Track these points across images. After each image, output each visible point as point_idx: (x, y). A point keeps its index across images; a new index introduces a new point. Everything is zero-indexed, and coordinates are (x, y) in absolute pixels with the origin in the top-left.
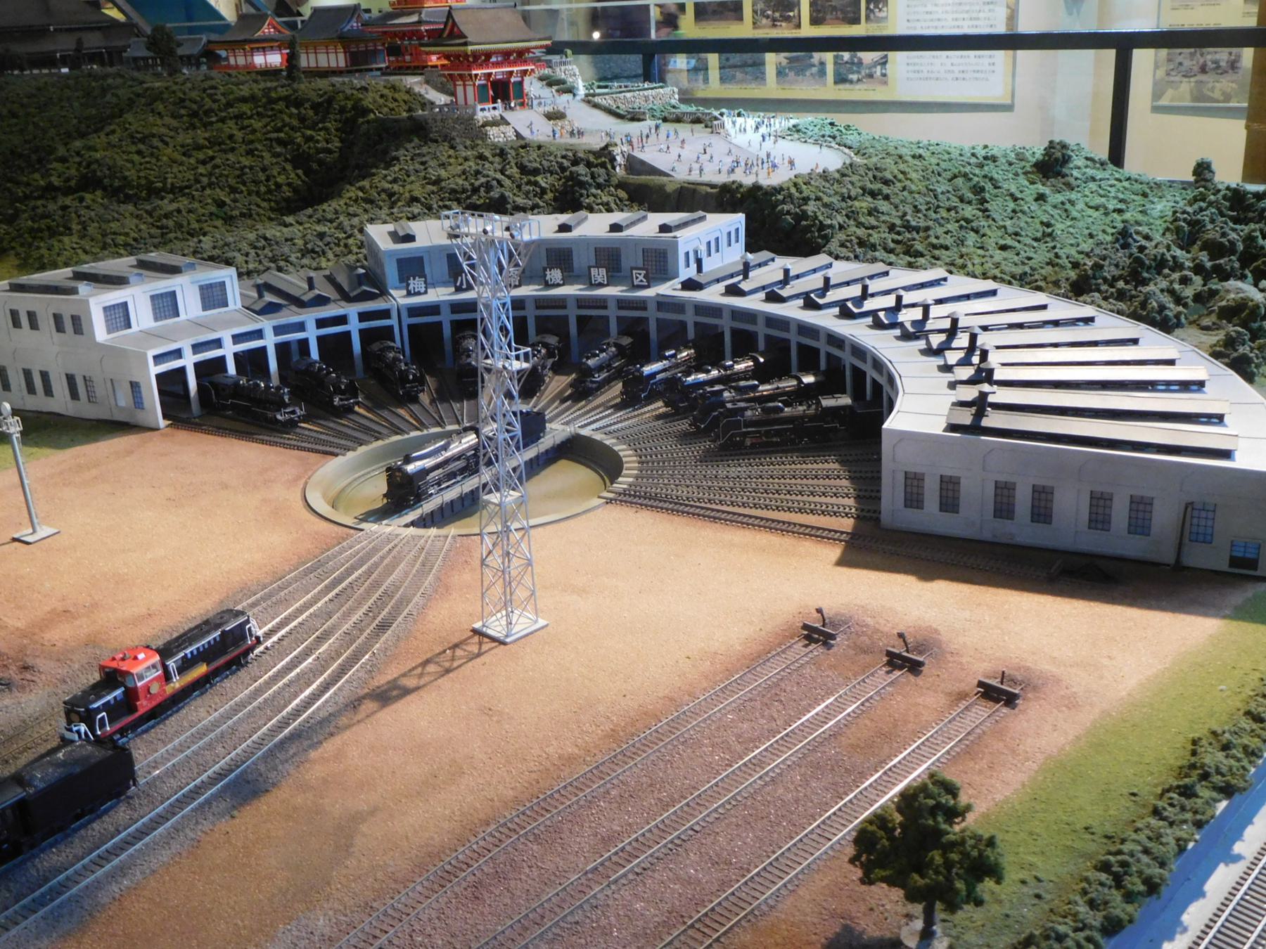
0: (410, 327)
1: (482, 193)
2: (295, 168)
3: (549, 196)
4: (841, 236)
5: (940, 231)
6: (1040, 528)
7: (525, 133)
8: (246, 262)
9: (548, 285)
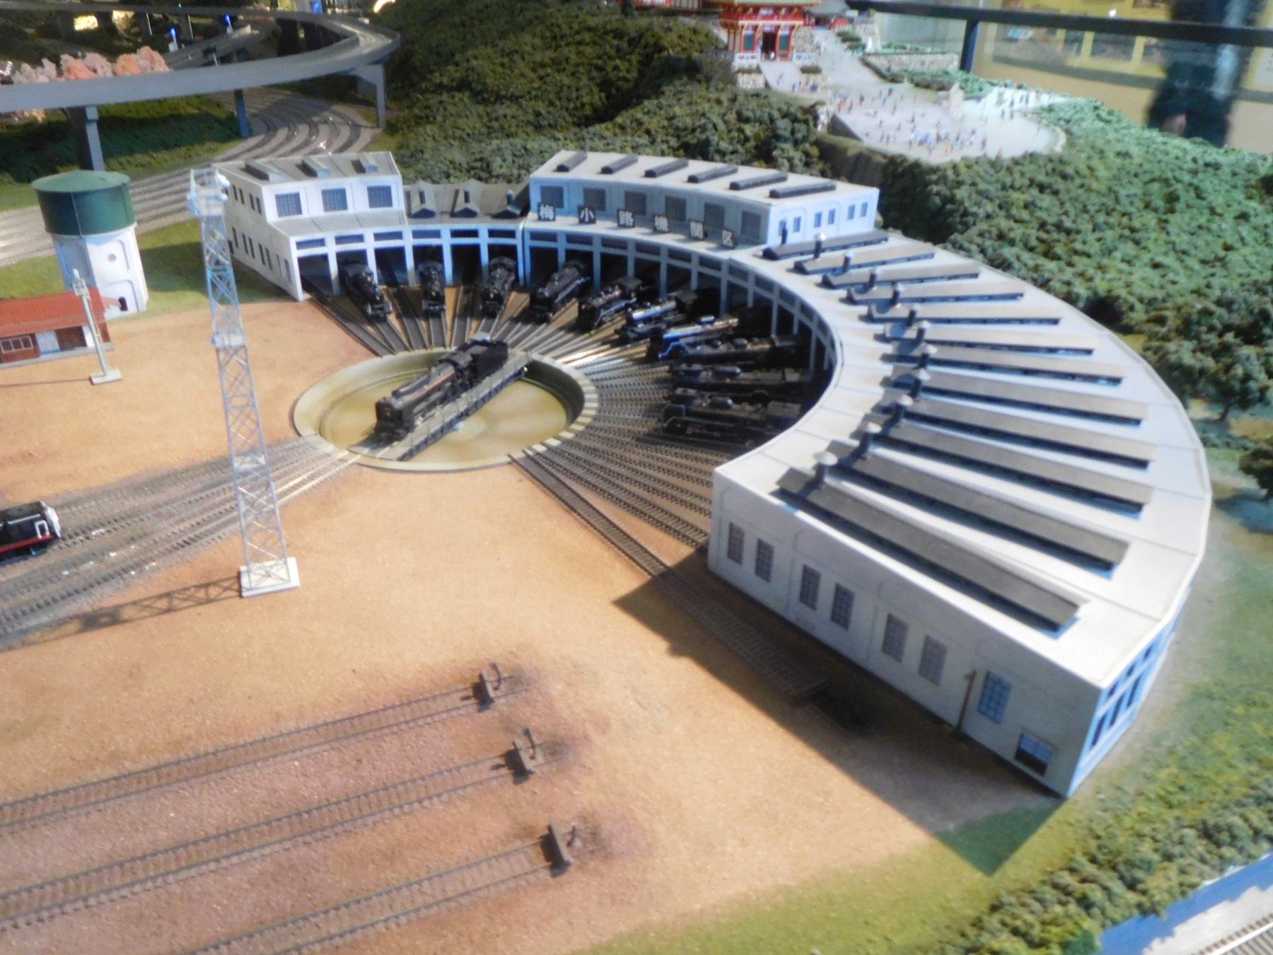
0: (533, 250)
1: (697, 133)
2: (601, 91)
3: (752, 143)
4: (983, 226)
5: (1092, 237)
6: (837, 628)
7: (772, 83)
9: (656, 231)
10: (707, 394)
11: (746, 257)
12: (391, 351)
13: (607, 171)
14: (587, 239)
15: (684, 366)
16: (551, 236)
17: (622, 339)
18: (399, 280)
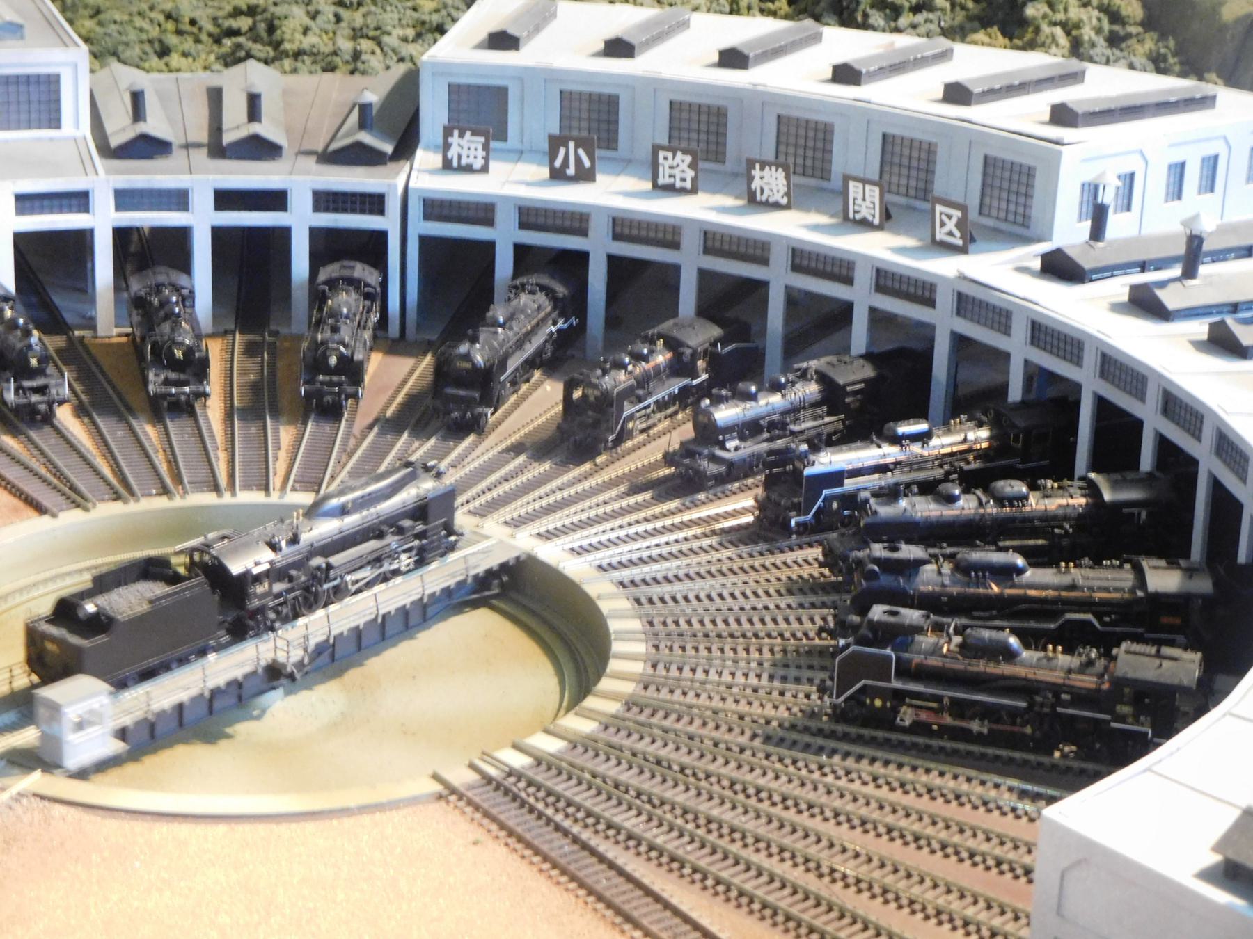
0: (427, 243)
8: (306, 31)
9: (755, 202)
10: (953, 623)
11: (1002, 271)
12: (77, 499)
13: (732, 58)
14: (576, 221)
15: (878, 550)
16: (482, 212)
17: (684, 479)
18: (69, 317)
